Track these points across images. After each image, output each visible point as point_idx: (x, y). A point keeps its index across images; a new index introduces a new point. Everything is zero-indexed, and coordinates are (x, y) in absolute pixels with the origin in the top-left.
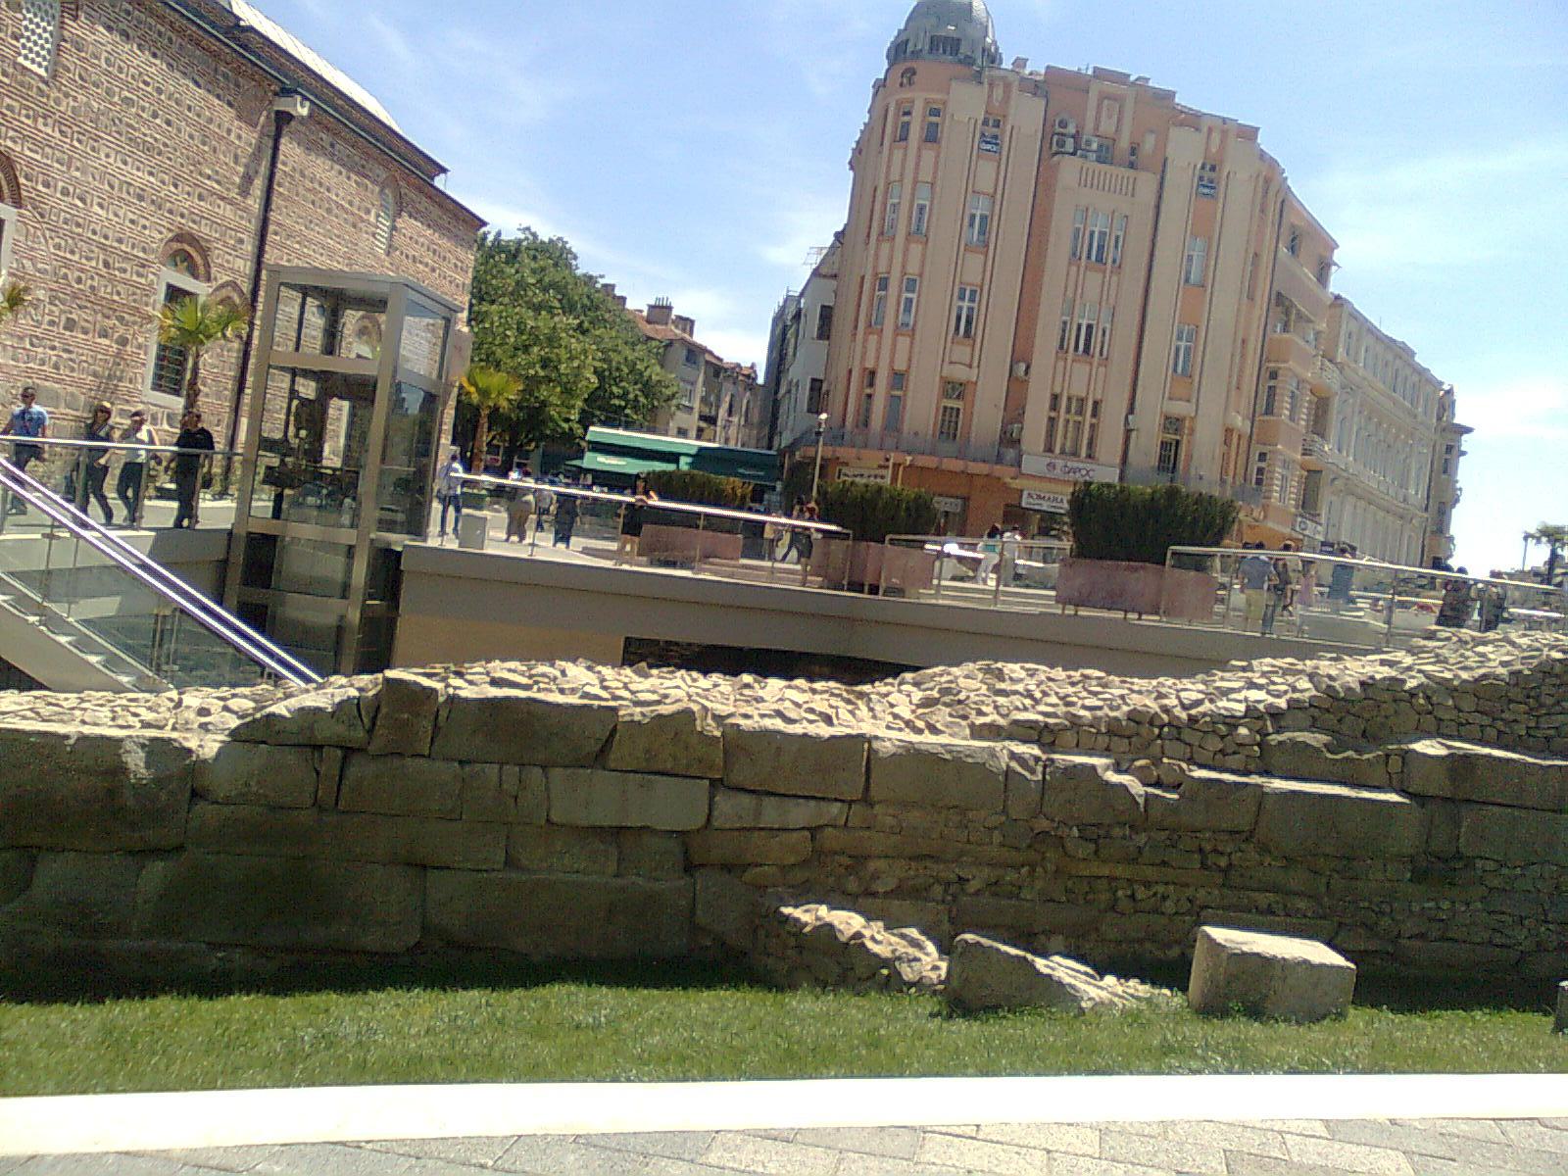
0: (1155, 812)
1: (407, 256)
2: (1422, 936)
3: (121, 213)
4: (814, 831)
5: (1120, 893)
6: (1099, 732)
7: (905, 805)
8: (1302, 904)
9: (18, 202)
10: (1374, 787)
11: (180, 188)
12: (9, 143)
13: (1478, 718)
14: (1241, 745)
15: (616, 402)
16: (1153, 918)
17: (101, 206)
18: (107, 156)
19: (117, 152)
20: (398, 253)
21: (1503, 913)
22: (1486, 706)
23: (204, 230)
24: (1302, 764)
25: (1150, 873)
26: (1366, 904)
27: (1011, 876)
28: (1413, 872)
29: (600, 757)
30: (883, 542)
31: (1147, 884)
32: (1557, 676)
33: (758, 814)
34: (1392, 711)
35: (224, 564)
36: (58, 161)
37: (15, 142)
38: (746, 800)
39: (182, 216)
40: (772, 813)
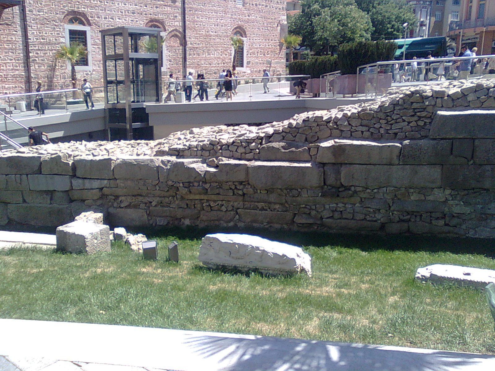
0: (207, 177)
1: (253, 5)
2: (332, 217)
3: (127, 19)
4: (101, 189)
5: (204, 205)
6: (198, 150)
7: (126, 179)
8: (277, 206)
9: (90, 25)
10: (307, 161)
11: (148, 7)
12: (83, 9)
13: (361, 128)
14: (251, 150)
15: (390, 30)
16: (219, 212)
17: (119, 19)
18: (118, 4)
19: (121, 2)
21: (369, 207)
22: (365, 122)
23: (160, 17)
24: (273, 155)
25: (213, 197)
26: (304, 206)
27: (167, 200)
28: (322, 193)
29: (40, 172)
30: (319, 77)
31: (215, 201)
32: (401, 105)
33: (84, 185)
34: (318, 130)
35: (105, 117)
36: (101, 10)
37: (85, 8)
38: (80, 181)
39: (151, 14)
40: (88, 184)
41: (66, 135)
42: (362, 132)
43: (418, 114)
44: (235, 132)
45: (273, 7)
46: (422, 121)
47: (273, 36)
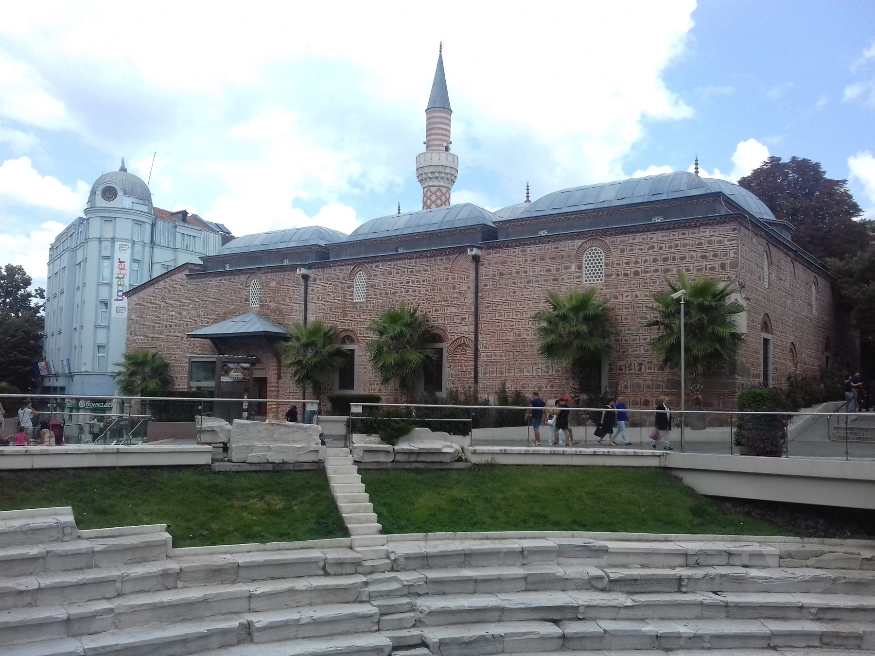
1: (626, 275)
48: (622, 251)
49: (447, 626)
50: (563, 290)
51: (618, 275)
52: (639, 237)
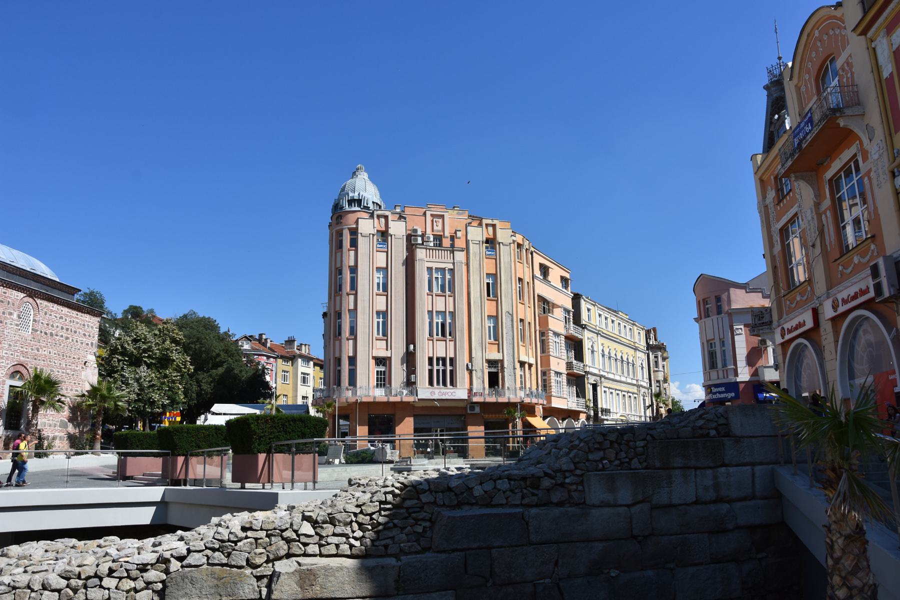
1: (46, 333)
13: (335, 540)
20: (38, 332)
41: (157, 522)
42: (337, 546)
43: (414, 515)
44: (156, 549)
45: (77, 341)
46: (420, 525)
47: (75, 383)
48: (46, 314)
49: (768, 256)
50: (5, 333)
51: (41, 332)
52: (56, 307)
